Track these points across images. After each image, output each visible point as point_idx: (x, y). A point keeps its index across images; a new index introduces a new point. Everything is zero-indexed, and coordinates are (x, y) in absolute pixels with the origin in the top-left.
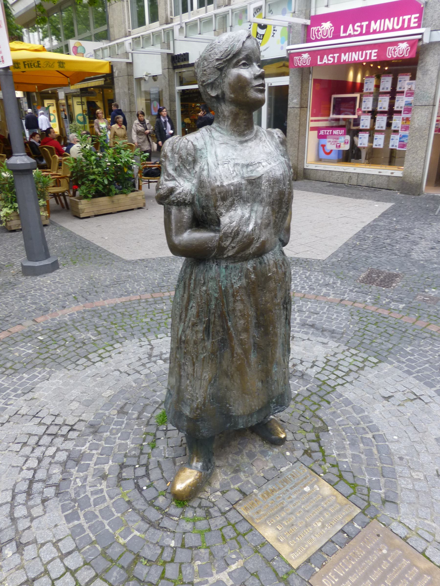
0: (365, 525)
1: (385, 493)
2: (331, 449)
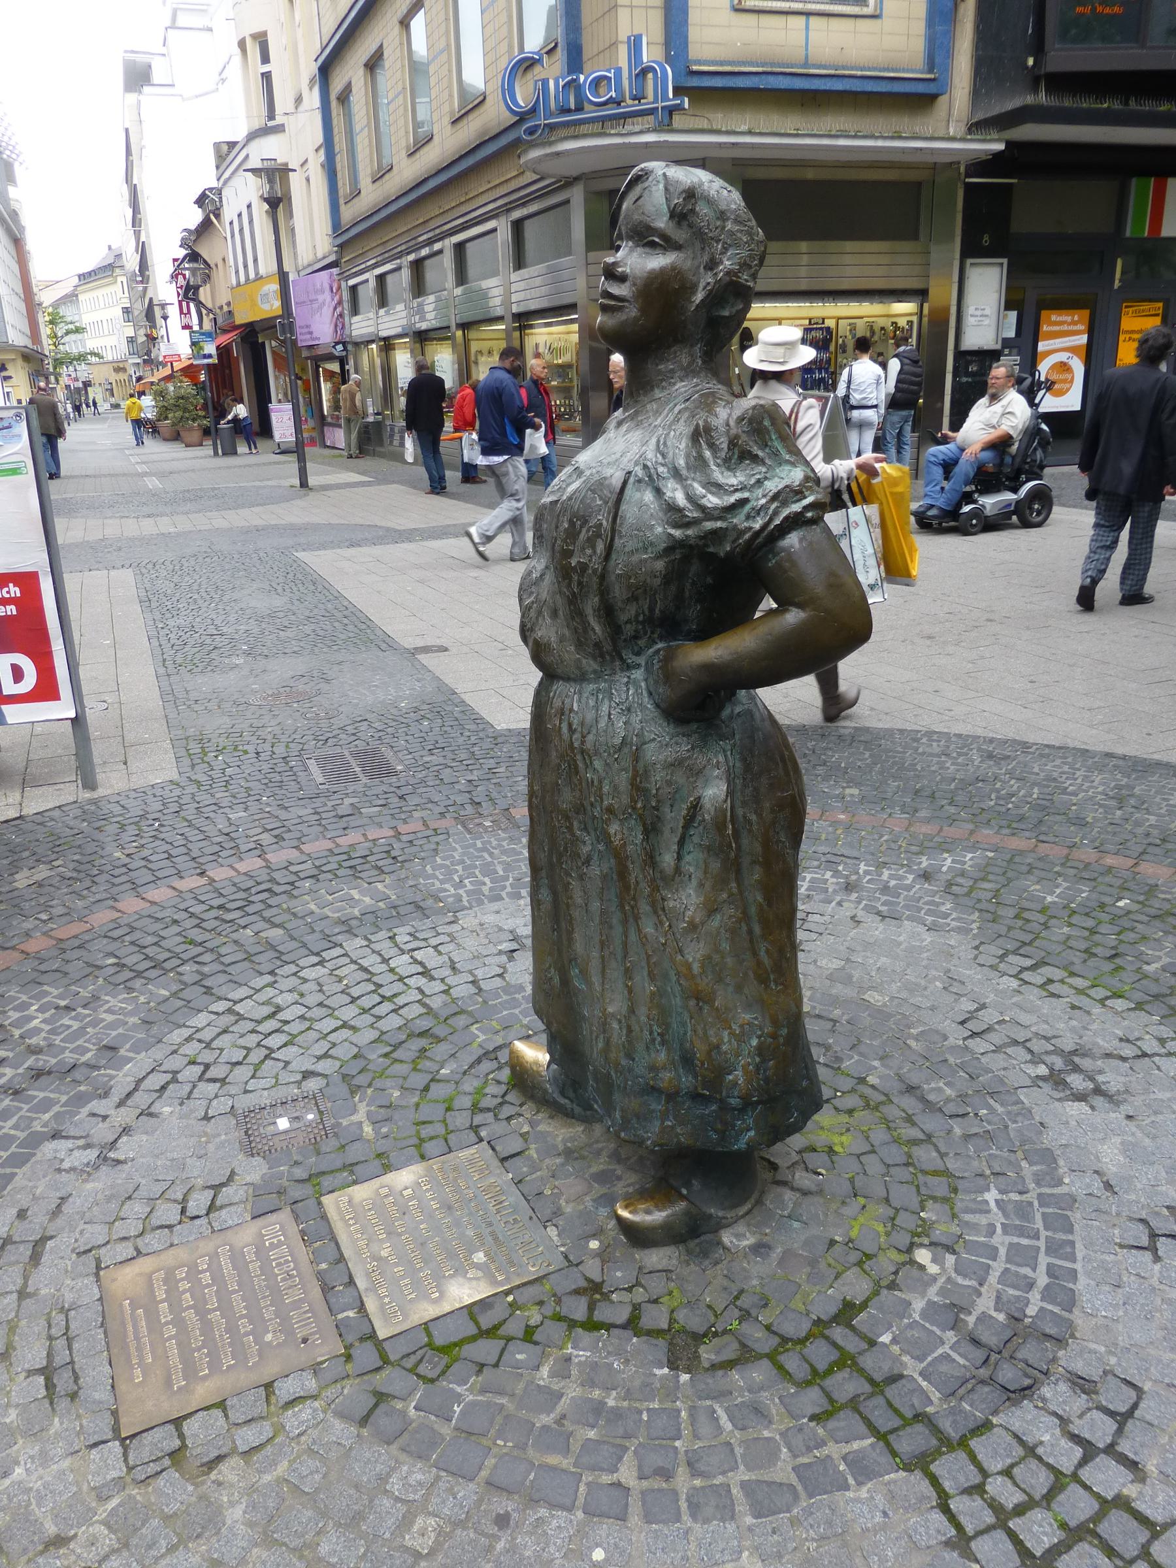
0: (340, 1329)
1: (403, 1413)
2: (594, 1348)
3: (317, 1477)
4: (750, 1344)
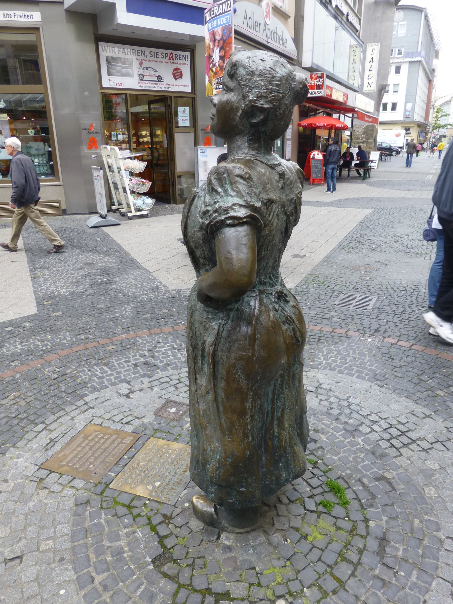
3: (52, 510)
4: (180, 575)
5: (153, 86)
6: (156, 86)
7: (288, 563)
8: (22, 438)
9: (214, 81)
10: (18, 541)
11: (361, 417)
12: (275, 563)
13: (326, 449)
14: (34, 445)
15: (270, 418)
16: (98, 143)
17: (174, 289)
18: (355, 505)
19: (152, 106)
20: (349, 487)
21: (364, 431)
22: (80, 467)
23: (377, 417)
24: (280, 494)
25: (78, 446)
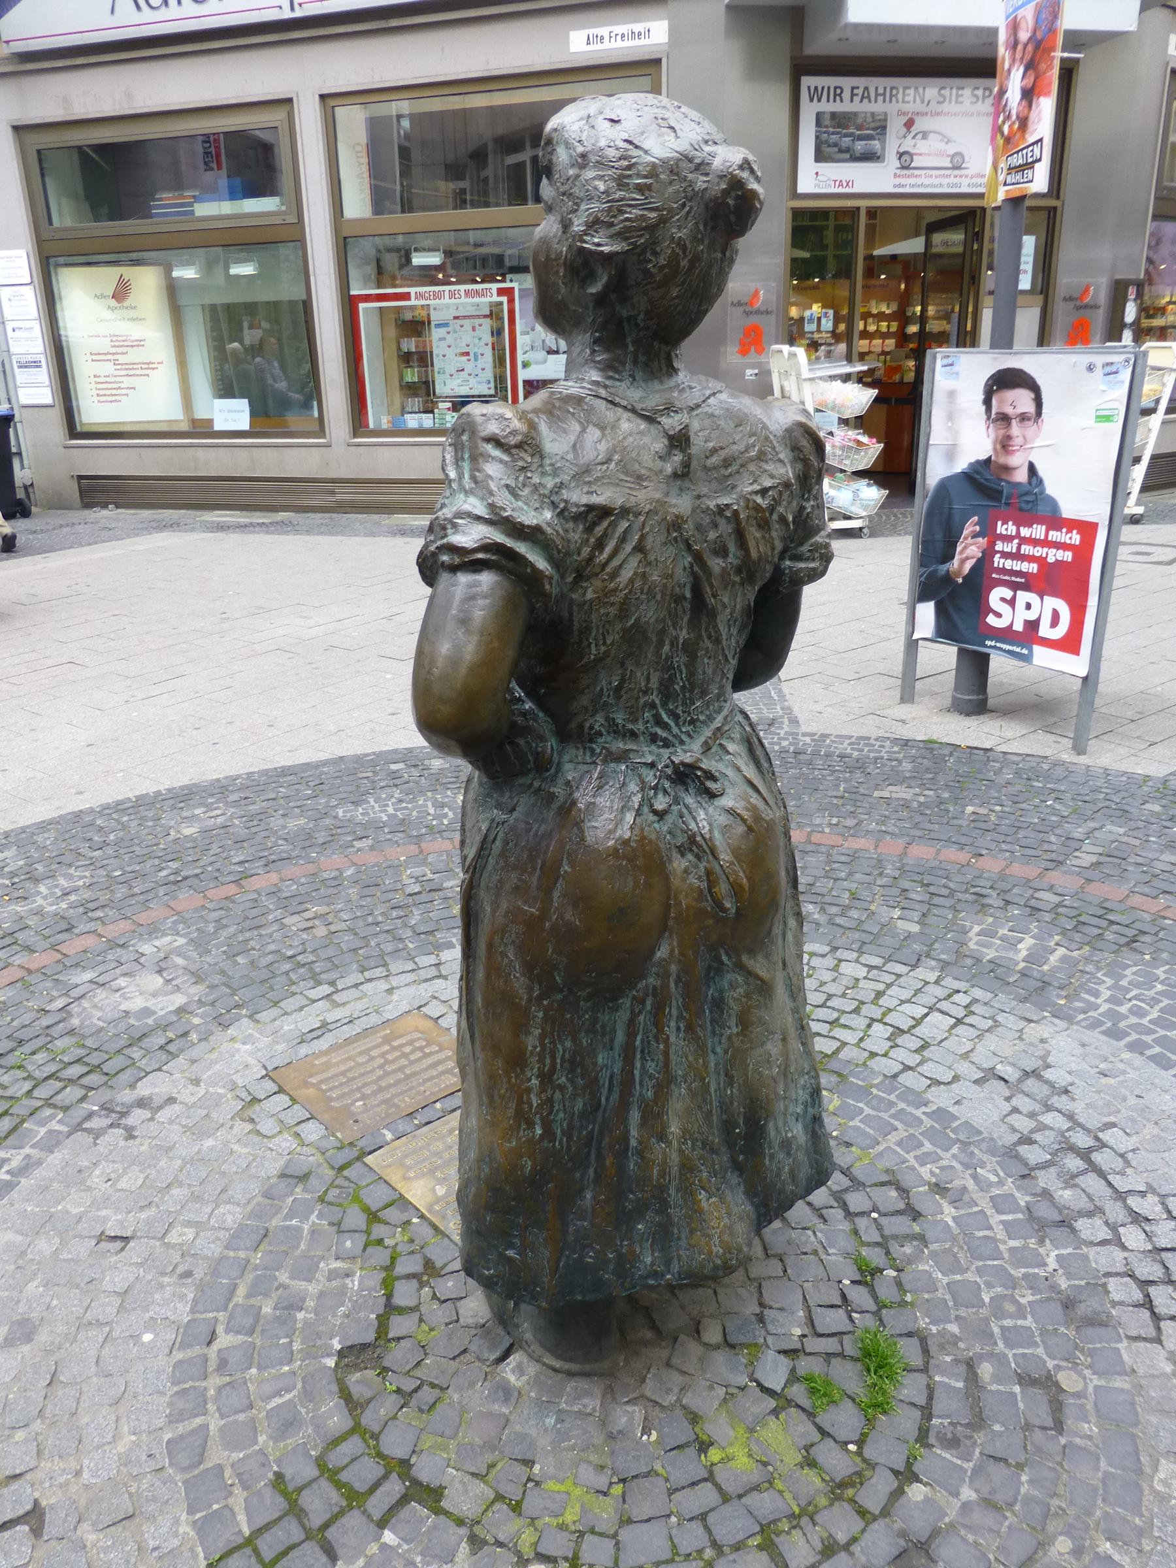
4: (371, 1406)
5: (937, 181)
6: (945, 181)
7: (617, 1490)
8: (276, 1004)
9: (1002, 165)
10: (142, 1208)
11: (1108, 1192)
12: (587, 1473)
13: (934, 1247)
14: (288, 1026)
15: (615, 1096)
16: (765, 338)
17: (814, 730)
18: (907, 1421)
19: (938, 238)
20: (925, 1370)
21: (1085, 1234)
22: (337, 1099)
23: (1158, 1208)
24: (711, 1316)
25: (362, 1053)
